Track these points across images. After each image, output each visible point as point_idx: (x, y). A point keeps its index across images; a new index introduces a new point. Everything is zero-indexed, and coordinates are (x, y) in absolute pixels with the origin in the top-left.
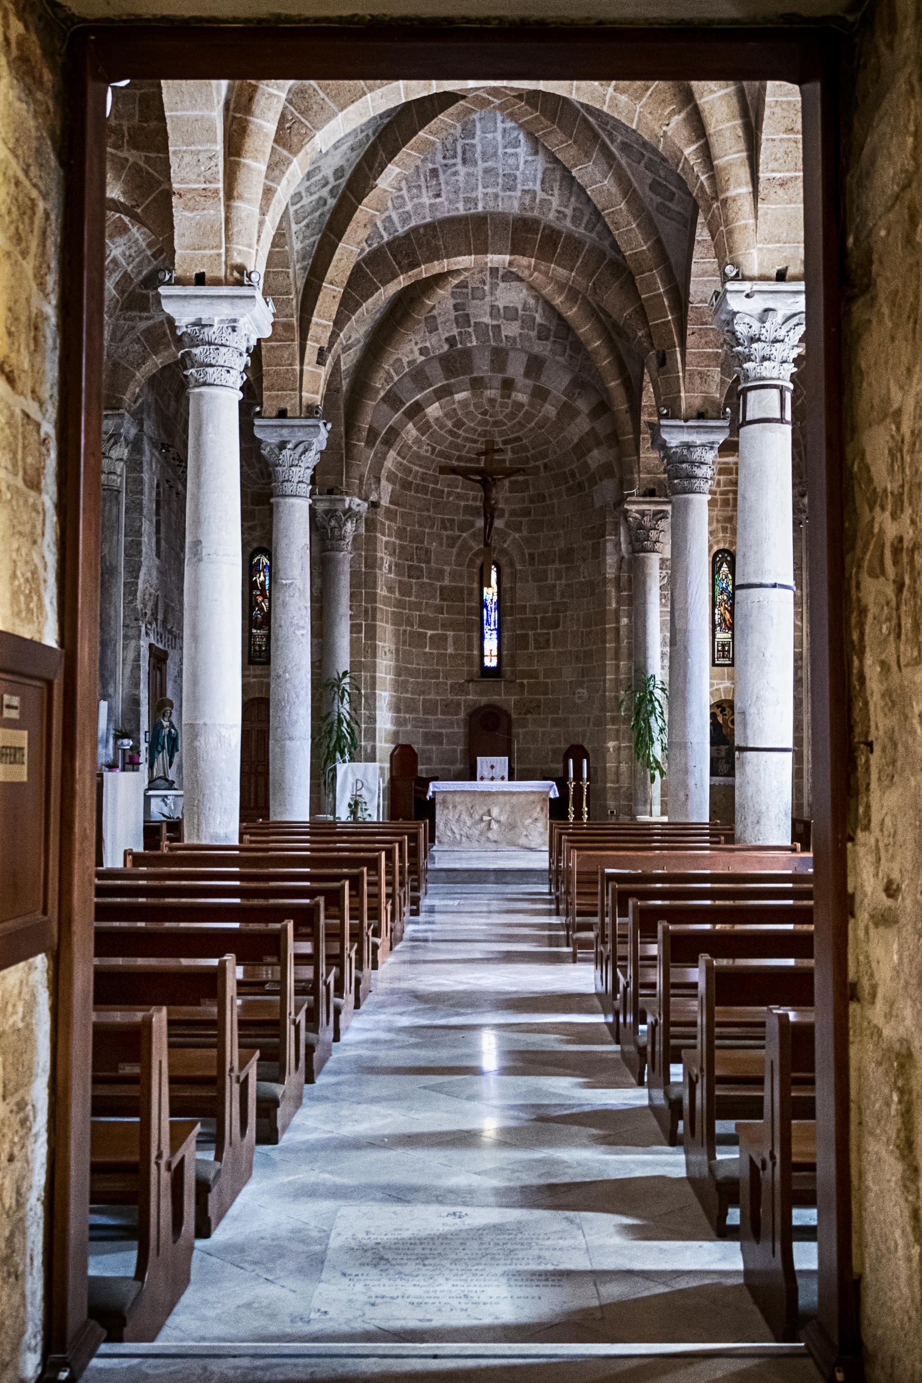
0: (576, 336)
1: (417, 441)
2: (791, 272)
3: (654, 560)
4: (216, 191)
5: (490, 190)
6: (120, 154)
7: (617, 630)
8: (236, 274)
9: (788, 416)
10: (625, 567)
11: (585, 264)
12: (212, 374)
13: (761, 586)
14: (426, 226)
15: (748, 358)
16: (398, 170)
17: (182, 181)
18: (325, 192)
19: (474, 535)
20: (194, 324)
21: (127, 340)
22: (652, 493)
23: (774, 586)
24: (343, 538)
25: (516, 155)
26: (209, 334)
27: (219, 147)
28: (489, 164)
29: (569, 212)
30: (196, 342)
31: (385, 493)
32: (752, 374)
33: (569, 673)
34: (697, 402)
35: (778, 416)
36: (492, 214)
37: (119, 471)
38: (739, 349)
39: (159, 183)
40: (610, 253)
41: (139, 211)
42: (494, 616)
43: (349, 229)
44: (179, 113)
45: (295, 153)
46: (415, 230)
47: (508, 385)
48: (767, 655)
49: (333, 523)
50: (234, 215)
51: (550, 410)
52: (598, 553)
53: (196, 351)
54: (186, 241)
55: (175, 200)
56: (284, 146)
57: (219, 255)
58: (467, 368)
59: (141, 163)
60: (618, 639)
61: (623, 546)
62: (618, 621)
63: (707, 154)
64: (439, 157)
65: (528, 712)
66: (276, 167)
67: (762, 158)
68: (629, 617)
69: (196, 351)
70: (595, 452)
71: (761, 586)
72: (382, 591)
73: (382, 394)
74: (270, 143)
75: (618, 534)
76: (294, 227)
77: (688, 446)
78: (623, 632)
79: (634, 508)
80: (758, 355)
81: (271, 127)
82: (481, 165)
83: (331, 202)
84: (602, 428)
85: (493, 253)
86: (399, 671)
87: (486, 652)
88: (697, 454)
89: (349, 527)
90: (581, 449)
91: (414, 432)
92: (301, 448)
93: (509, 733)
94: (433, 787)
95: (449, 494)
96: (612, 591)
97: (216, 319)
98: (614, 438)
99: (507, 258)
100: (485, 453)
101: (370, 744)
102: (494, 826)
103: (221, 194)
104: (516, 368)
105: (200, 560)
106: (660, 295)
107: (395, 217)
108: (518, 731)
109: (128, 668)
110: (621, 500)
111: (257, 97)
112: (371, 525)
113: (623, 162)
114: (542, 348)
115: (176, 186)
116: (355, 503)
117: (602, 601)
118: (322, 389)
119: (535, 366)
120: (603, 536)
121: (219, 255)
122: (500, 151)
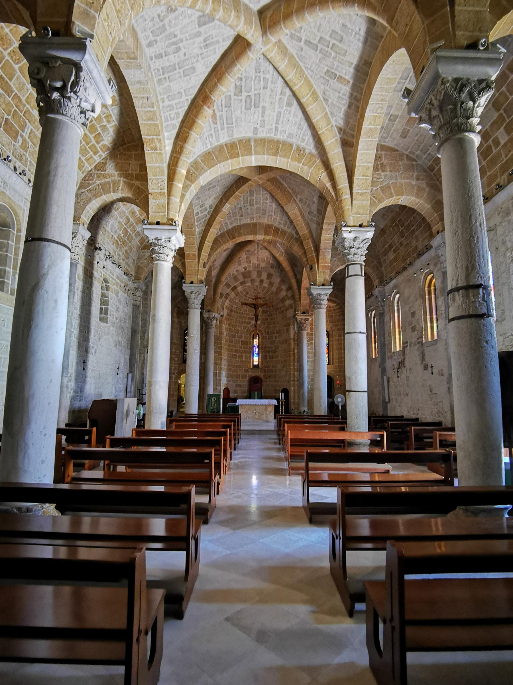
0: (283, 267)
1: (235, 298)
2: (364, 224)
3: (305, 333)
4: (164, 193)
5: (258, 215)
6: (132, 182)
7: (294, 353)
8: (170, 222)
9: (363, 274)
10: (296, 335)
11: (287, 238)
12: (193, 306)
13: (355, 333)
14: (238, 226)
15: (349, 254)
16: (229, 206)
17: (153, 189)
18: (206, 213)
19: (251, 326)
20: (155, 239)
21: (143, 259)
22: (304, 313)
23: (360, 333)
24: (212, 325)
25: (266, 203)
26: (161, 242)
27: (166, 178)
28: (258, 206)
29: (282, 222)
30: (156, 245)
31: (225, 312)
32: (350, 260)
33: (279, 366)
34: (322, 281)
35: (360, 274)
36: (259, 223)
37: (139, 300)
38: (346, 251)
39: (145, 192)
40: (295, 235)
41: (138, 201)
42: (257, 350)
43: (214, 224)
44: (151, 165)
45: (193, 183)
46: (234, 227)
47: (262, 281)
48: (358, 358)
49: (209, 321)
50: (170, 201)
51: (274, 289)
52: (288, 331)
53: (156, 248)
54: (154, 210)
55: (150, 196)
56: (189, 180)
57: (165, 215)
58: (250, 276)
59: (139, 185)
60: (294, 356)
61: (296, 329)
62: (294, 351)
63: (334, 185)
64: (242, 203)
65: (267, 378)
66: (186, 187)
67: (354, 185)
68: (297, 349)
69: (156, 248)
70: (287, 301)
71: (355, 333)
72: (224, 341)
73: (225, 283)
74: (183, 179)
75: (294, 325)
76: (196, 224)
77: (320, 295)
78: (296, 355)
79: (299, 317)
80: (353, 253)
81: (184, 172)
82: (255, 206)
83: (208, 216)
84: (290, 294)
85: (259, 234)
86: (228, 366)
87: (254, 360)
88: (322, 297)
89: (214, 322)
90: (283, 300)
91: (234, 295)
92: (198, 293)
93: (262, 384)
94: (239, 402)
95: (244, 313)
96: (292, 341)
97: (163, 237)
98: (293, 297)
99: (263, 236)
100: (255, 299)
101: (219, 387)
102: (257, 413)
103: (166, 194)
104: (264, 276)
105: (155, 322)
106: (310, 248)
107: (228, 222)
108: (264, 383)
109: (141, 363)
110: (295, 315)
111: (179, 161)
112: (221, 322)
113: (300, 206)
114: (272, 271)
115: (150, 191)
116: (215, 314)
117: (289, 345)
118: (205, 275)
119: (270, 276)
120: (289, 326)
121: (165, 215)
122: (261, 202)
